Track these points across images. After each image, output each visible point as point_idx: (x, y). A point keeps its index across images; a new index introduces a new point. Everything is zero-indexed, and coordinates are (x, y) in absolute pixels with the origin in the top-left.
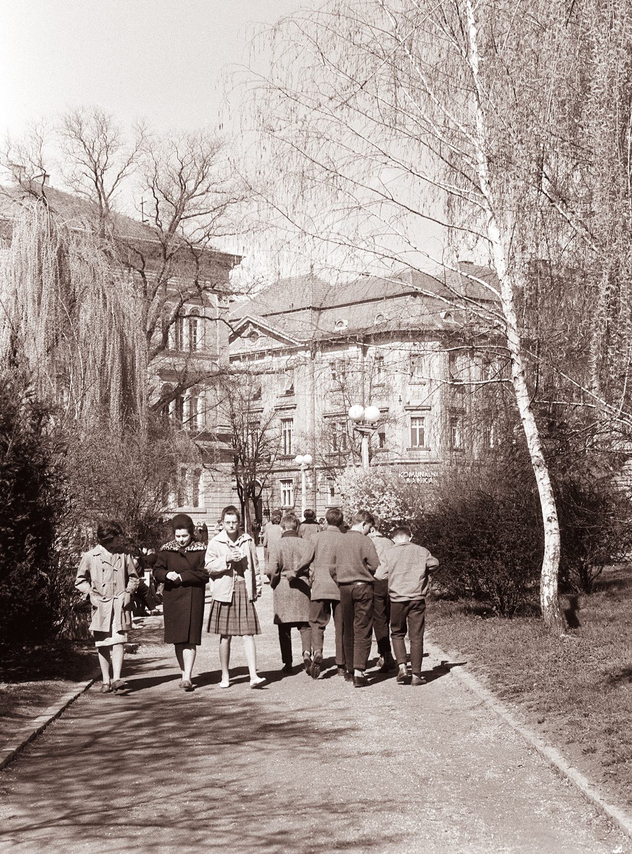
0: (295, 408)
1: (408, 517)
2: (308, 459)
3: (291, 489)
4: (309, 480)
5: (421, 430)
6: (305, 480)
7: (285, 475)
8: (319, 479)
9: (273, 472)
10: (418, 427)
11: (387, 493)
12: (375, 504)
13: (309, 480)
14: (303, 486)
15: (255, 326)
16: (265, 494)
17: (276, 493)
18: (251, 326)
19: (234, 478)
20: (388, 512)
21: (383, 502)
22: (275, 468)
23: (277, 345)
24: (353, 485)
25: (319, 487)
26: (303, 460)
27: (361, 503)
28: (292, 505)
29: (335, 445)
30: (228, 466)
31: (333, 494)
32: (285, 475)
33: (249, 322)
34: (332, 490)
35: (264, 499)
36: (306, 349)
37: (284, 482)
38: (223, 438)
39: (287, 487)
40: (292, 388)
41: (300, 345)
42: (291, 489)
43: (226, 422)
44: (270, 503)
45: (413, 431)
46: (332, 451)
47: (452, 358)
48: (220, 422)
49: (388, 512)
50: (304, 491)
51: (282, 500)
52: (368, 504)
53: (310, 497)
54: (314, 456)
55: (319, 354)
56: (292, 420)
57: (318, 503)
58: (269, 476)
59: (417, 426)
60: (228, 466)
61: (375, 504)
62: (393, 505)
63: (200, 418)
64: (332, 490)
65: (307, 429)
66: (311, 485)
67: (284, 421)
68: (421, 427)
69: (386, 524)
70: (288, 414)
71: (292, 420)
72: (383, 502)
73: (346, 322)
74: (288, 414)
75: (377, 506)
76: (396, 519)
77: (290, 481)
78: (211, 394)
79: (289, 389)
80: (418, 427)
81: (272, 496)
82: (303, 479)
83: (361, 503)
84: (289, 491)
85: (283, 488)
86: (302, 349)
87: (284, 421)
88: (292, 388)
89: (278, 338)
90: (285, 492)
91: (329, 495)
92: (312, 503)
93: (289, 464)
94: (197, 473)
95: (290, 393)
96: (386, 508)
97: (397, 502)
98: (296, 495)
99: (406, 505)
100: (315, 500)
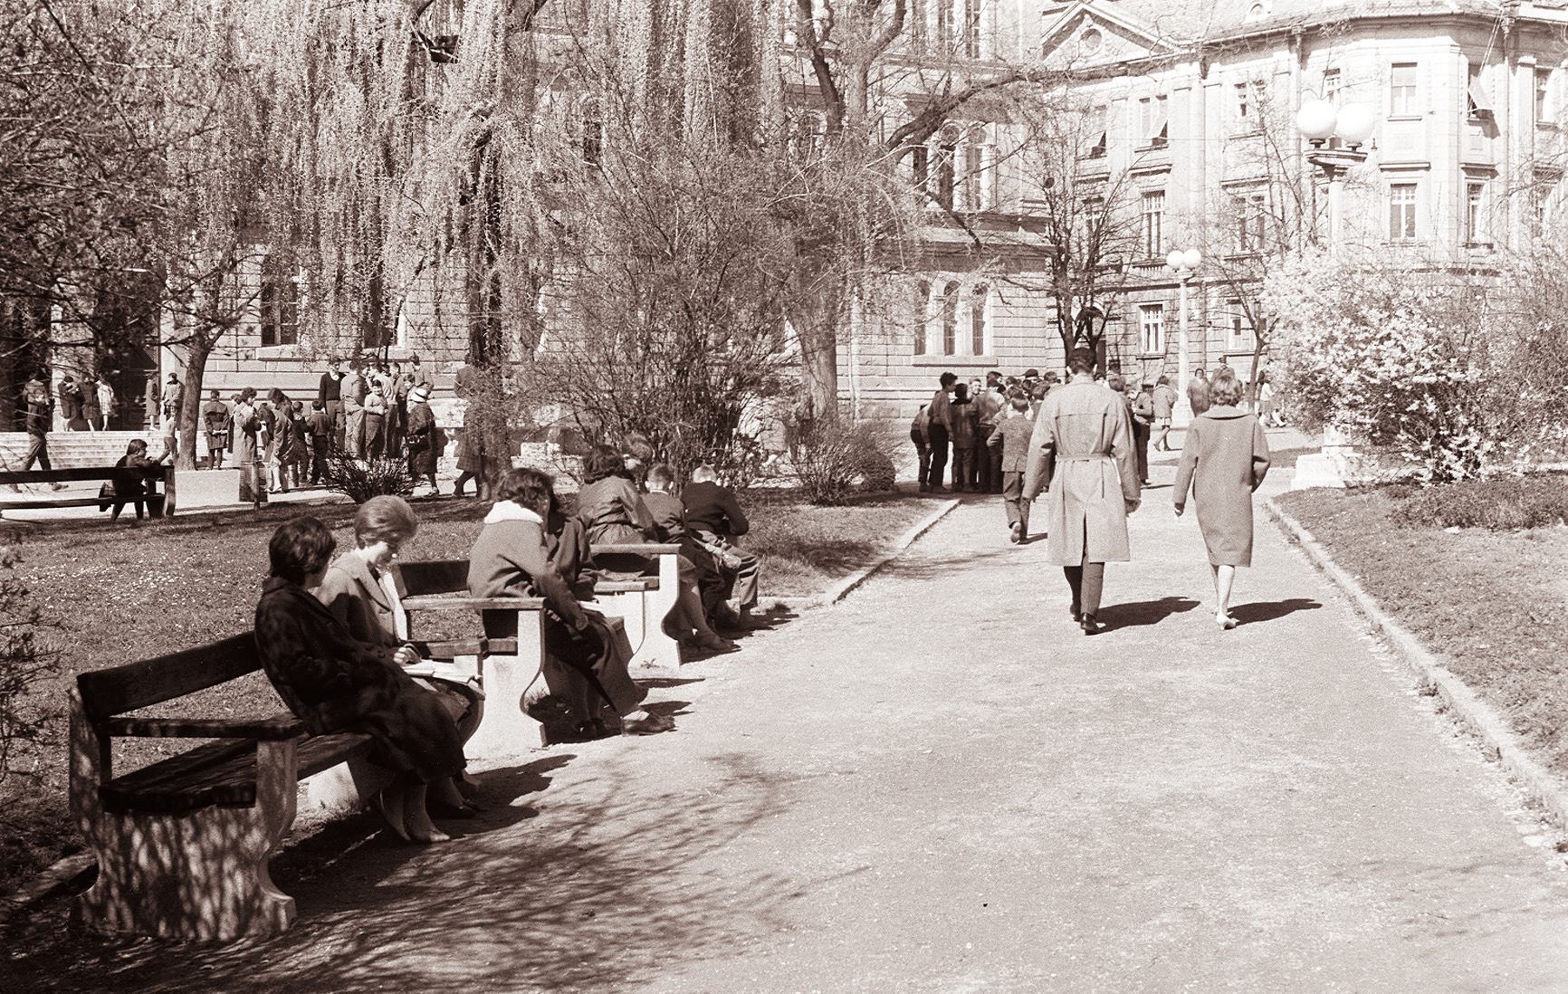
0: (1168, 171)
1: (1456, 376)
2: (1193, 257)
3: (1159, 321)
4: (1194, 303)
5: (1411, 208)
6: (1186, 302)
7: (1149, 296)
8: (1213, 303)
9: (1127, 290)
10: (1403, 203)
11: (1401, 312)
12: (1367, 341)
13: (1194, 303)
14: (1182, 316)
15: (1096, 18)
16: (1112, 331)
17: (1132, 329)
18: (1088, 20)
19: (1053, 301)
20: (1403, 363)
21: (1388, 337)
22: (1130, 283)
23: (1136, 53)
24: (1309, 291)
25: (1211, 316)
26: (1182, 259)
27: (1332, 340)
28: (1162, 350)
29: (1243, 238)
30: (1041, 278)
31: (1238, 330)
32: (1149, 296)
33: (1084, 12)
34: (1237, 322)
35: (1109, 340)
36: (1190, 59)
37: (1146, 308)
38: (1032, 224)
39: (1152, 318)
40: (1164, 132)
41: (1177, 51)
42: (1159, 321)
43: (1038, 194)
44: (1122, 349)
45: (1395, 209)
46: (1238, 250)
47: (1474, 69)
48: (1020, 188)
49: (1403, 363)
50: (1183, 323)
51: (1144, 342)
52: (1350, 341)
53: (1194, 336)
54: (1202, 247)
55: (1214, 67)
56: (1163, 193)
57: (1210, 346)
58: (1120, 298)
59: (1403, 198)
60: (1041, 278)
61: (1367, 341)
62: (1419, 342)
63: (985, 180)
64: (1237, 322)
65: (1192, 201)
66: (1197, 314)
67: (1148, 195)
68: (1410, 202)
69: (1396, 391)
70: (1156, 182)
71: (1163, 193)
72: (1388, 337)
73: (1267, 6)
74: (1156, 182)
75: (1372, 347)
76: (1426, 379)
77: (1158, 307)
78: (1003, 136)
79: (1157, 135)
80: (1403, 203)
81: (1125, 335)
82: (1183, 304)
83: (1332, 340)
84: (1156, 325)
85: (1146, 318)
86: (1183, 59)
87: (1148, 195)
88: (1164, 132)
89: (1143, 42)
90: (1147, 326)
91: (1232, 332)
92: (1198, 347)
93: (1155, 274)
94: (981, 290)
95: (1160, 143)
96: (1398, 353)
97: (1427, 336)
98: (1169, 334)
99: (1449, 347)
100: (1204, 341)
